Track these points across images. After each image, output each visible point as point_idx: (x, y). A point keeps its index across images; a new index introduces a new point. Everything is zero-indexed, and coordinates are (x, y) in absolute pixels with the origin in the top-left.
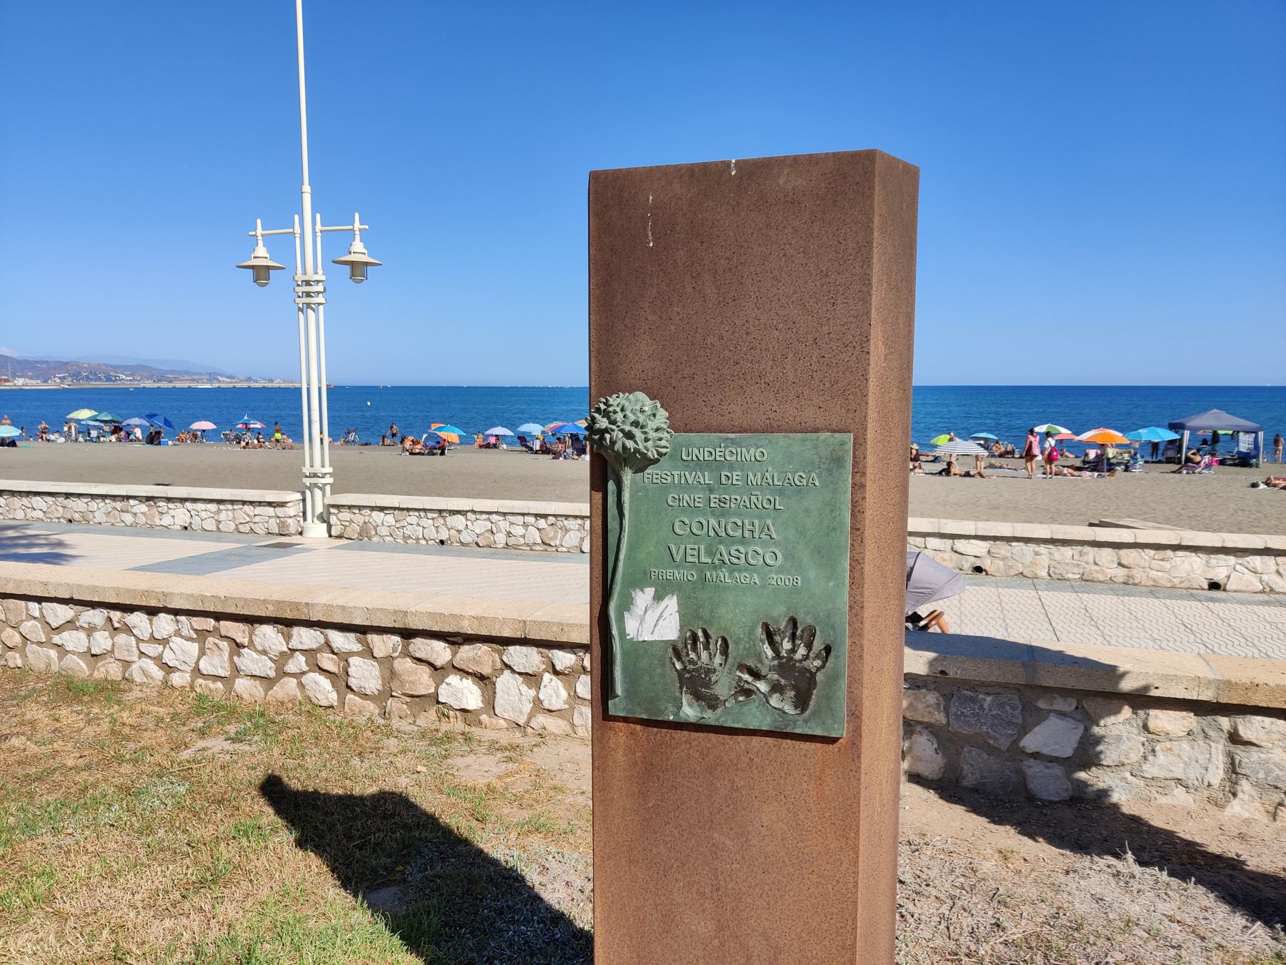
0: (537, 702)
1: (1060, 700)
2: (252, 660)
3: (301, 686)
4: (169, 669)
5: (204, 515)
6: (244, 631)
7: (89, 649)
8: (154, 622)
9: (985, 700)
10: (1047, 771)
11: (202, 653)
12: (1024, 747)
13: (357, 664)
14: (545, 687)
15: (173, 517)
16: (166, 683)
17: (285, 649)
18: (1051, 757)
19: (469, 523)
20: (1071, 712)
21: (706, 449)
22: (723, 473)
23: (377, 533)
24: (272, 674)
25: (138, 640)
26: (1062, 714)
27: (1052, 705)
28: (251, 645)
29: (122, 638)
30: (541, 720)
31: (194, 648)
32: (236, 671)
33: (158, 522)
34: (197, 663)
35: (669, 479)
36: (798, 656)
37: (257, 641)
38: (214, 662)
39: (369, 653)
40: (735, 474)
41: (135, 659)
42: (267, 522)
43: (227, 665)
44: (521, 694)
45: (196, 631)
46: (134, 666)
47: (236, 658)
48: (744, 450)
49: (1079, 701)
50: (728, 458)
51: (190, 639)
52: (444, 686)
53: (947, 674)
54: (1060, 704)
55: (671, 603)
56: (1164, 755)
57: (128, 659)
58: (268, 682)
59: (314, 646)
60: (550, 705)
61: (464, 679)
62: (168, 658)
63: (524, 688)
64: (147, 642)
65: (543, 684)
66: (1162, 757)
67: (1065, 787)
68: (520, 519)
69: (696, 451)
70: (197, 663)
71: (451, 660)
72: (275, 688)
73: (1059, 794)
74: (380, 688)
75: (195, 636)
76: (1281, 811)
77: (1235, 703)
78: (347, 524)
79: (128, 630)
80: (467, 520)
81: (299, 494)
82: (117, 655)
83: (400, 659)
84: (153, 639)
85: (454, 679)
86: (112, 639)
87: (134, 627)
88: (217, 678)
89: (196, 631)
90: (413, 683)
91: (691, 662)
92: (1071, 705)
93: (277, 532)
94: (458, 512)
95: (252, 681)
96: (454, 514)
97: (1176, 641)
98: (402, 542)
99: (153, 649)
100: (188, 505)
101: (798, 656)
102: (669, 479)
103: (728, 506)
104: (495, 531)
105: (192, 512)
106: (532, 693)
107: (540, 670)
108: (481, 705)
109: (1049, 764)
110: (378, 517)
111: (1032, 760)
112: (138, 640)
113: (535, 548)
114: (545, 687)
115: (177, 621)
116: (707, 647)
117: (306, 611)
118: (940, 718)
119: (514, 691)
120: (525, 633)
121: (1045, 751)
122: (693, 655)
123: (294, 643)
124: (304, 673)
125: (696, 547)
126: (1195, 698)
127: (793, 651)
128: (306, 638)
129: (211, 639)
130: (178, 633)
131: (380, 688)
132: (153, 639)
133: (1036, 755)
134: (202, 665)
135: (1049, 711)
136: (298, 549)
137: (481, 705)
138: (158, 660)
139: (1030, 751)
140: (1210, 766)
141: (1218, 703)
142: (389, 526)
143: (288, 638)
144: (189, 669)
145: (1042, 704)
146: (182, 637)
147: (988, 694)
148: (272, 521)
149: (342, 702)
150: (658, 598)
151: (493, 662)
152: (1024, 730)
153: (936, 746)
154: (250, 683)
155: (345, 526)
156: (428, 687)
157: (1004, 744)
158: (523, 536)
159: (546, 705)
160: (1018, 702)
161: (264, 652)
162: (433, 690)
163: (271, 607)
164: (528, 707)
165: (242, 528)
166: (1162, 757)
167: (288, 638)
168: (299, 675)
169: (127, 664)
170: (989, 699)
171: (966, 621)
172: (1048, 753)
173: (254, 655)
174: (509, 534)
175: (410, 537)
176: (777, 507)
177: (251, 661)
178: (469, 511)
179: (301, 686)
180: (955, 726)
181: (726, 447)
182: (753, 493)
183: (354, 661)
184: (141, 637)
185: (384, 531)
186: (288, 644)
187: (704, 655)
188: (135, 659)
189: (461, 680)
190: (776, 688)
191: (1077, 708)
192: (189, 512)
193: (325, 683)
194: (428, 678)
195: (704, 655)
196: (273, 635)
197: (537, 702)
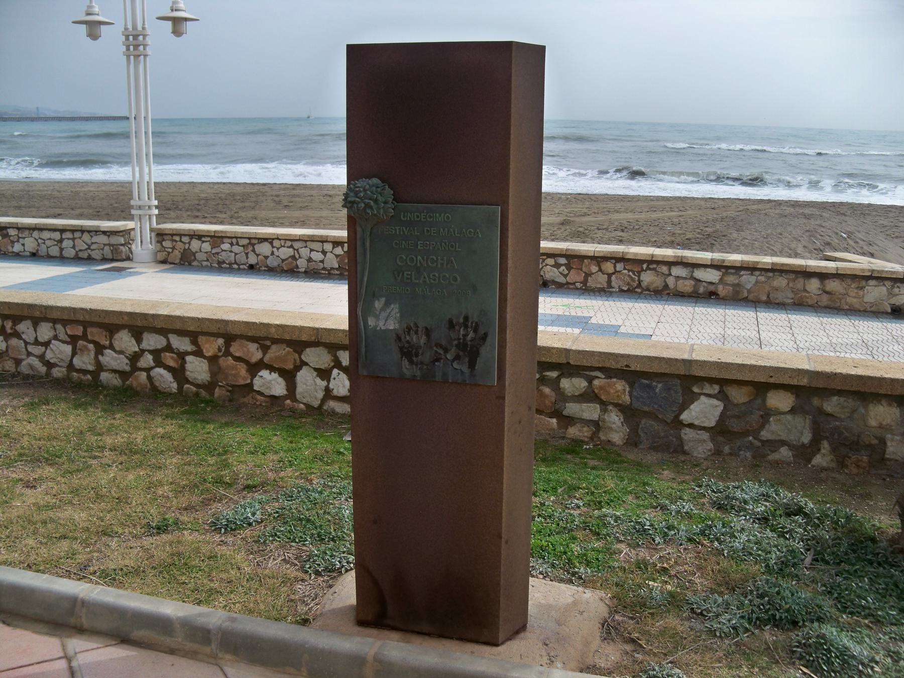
0: (328, 390)
1: (707, 385)
2: (113, 358)
3: (149, 378)
4: (49, 365)
5: (49, 243)
6: (106, 336)
7: (36, 339)
8: (38, 329)
9: (657, 386)
10: (697, 436)
11: (74, 353)
12: (682, 420)
13: (191, 361)
14: (334, 379)
15: (23, 245)
16: (48, 374)
17: (137, 349)
18: (701, 426)
19: (275, 250)
20: (715, 395)
21: (415, 214)
22: (426, 229)
23: (195, 258)
24: (128, 368)
25: (26, 343)
26: (709, 396)
27: (702, 389)
28: (111, 347)
29: (14, 342)
30: (332, 404)
31: (68, 349)
32: (100, 367)
33: (10, 249)
34: (71, 360)
35: (394, 231)
36: (469, 338)
37: (117, 344)
38: (83, 360)
39: (198, 353)
40: (432, 229)
41: (24, 357)
42: (103, 249)
43: (93, 362)
44: (316, 384)
45: (70, 336)
46: (24, 363)
47: (100, 357)
48: (437, 215)
49: (721, 387)
50: (428, 219)
51: (64, 342)
52: (257, 378)
53: (630, 367)
54: (708, 389)
55: (395, 309)
56: (775, 424)
57: (19, 357)
58: (123, 374)
59: (159, 347)
60: (338, 392)
61: (273, 373)
62: (49, 356)
63: (318, 380)
64: (33, 344)
65: (332, 377)
66: (774, 426)
67: (709, 448)
68: (317, 246)
69: (409, 214)
70: (71, 360)
71: (263, 358)
72: (130, 379)
73: (705, 453)
74: (209, 379)
75: (69, 340)
76: (847, 460)
77: (821, 387)
78: (170, 250)
79: (17, 335)
80: (273, 247)
81: (562, 385)
82: (12, 355)
83: (223, 358)
84: (37, 342)
85: (264, 373)
86: (7, 342)
87: (23, 333)
88: (85, 372)
89: (70, 336)
90: (234, 375)
91: (408, 342)
92: (715, 389)
93: (111, 257)
94: (265, 240)
95: (113, 374)
96: (261, 242)
97: (889, 356)
98: (217, 266)
99: (37, 350)
100: (36, 234)
101: (469, 338)
102: (394, 231)
103: (428, 248)
104: (297, 256)
105: (39, 240)
106: (324, 383)
107: (330, 366)
108: (285, 392)
109: (699, 432)
110: (195, 245)
111: (687, 429)
112: (26, 343)
113: (332, 272)
114: (334, 379)
115: (55, 329)
116: (416, 333)
117: (151, 320)
118: (627, 399)
119: (310, 382)
120: (318, 338)
121: (696, 423)
122: (408, 338)
123: (145, 345)
124: (152, 368)
125: (410, 273)
126: (796, 384)
127: (465, 336)
128: (152, 341)
129: (81, 342)
130: (56, 338)
131: (209, 379)
132: (37, 342)
133: (691, 426)
134: (76, 361)
135: (700, 394)
136: (130, 272)
137: (285, 392)
138: (41, 357)
139: (686, 423)
140: (804, 431)
141: (810, 387)
142: (206, 253)
143: (139, 340)
144: (65, 365)
145: (696, 389)
146: (60, 341)
147: (658, 382)
148: (107, 248)
149: (180, 388)
150: (387, 304)
151: (295, 359)
152: (684, 407)
153: (622, 420)
154: (111, 376)
155: (169, 253)
156: (245, 379)
157: (669, 417)
158: (322, 261)
159: (335, 393)
160: (679, 387)
161: (121, 352)
162: (249, 381)
163: (126, 318)
164: (320, 395)
165: (81, 255)
166: (774, 426)
167: (139, 340)
168: (148, 370)
169: (18, 362)
170: (660, 385)
171: (693, 336)
172: (699, 424)
173: (115, 355)
174: (310, 260)
175: (224, 262)
176: (457, 249)
177: (109, 358)
178: (275, 239)
179: (149, 378)
180: (637, 405)
181: (427, 213)
182: (444, 241)
183: (189, 358)
184: (28, 340)
185: (201, 256)
186: (139, 346)
187: (415, 337)
188: (24, 357)
189: (270, 373)
190: (457, 358)
191: (720, 392)
192: (37, 240)
193: (168, 376)
194: (245, 372)
195: (415, 337)
196: (128, 339)
197: (328, 390)
